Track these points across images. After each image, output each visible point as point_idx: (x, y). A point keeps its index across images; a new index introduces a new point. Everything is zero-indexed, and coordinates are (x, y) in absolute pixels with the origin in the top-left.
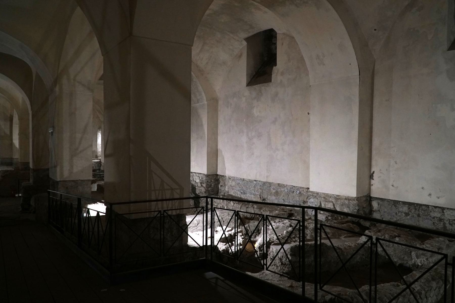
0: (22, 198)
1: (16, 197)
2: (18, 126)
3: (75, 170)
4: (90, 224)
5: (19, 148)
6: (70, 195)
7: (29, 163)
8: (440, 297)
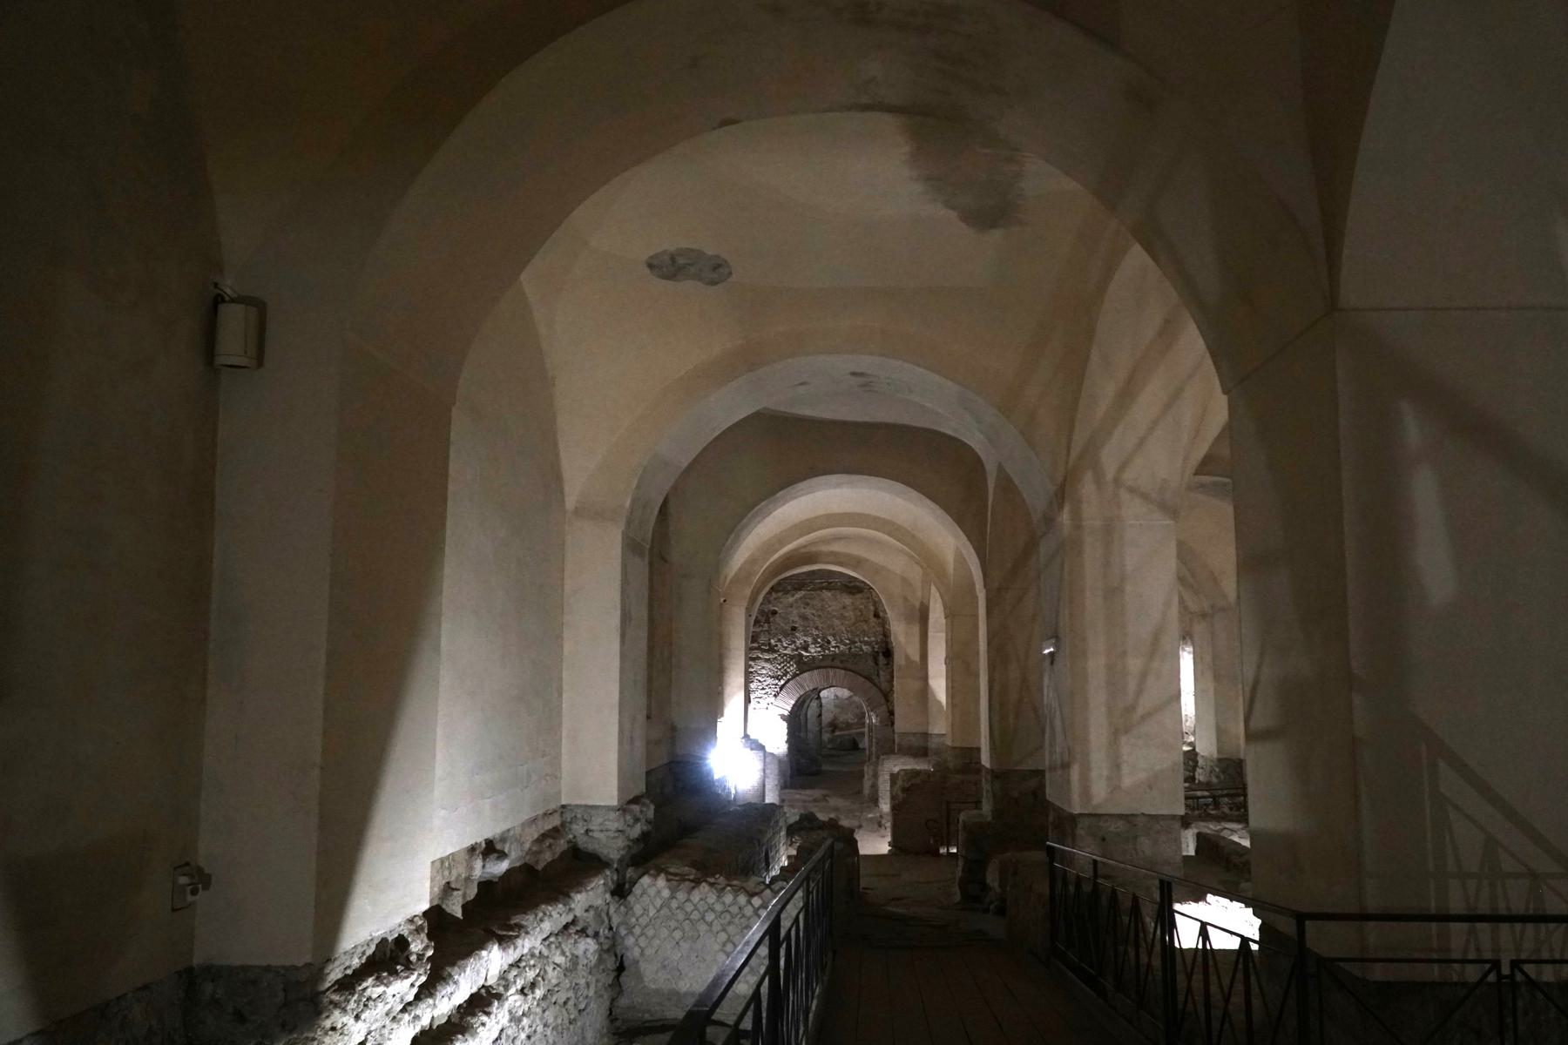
0: (961, 863)
1: (942, 855)
2: (944, 635)
3: (1127, 782)
4: (1213, 978)
5: (947, 703)
6: (1111, 861)
7: (979, 749)
8: (618, 964)
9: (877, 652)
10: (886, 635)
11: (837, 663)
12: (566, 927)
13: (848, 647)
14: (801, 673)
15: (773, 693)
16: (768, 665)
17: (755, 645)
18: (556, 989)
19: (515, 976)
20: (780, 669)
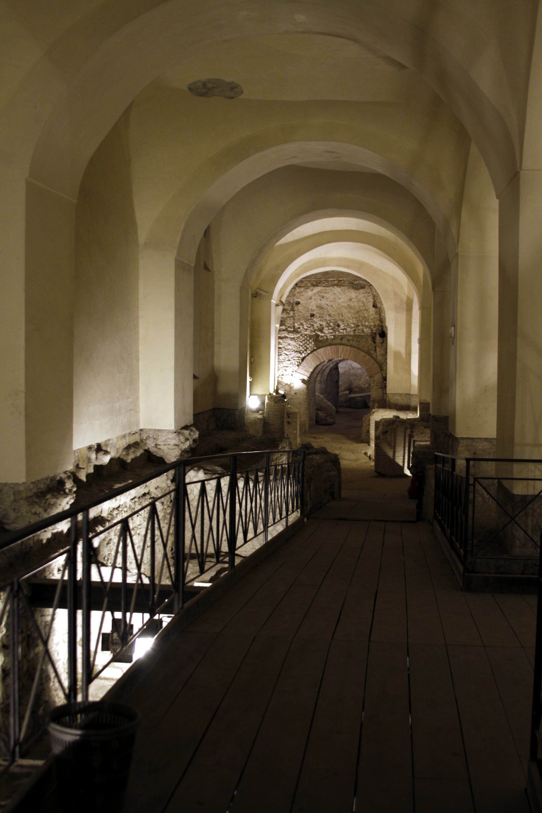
9: (375, 333)
10: (382, 321)
11: (345, 341)
12: (144, 495)
13: (354, 329)
14: (318, 349)
15: (297, 364)
16: (292, 343)
17: (283, 327)
18: (139, 527)
19: (117, 514)
20: (302, 346)
